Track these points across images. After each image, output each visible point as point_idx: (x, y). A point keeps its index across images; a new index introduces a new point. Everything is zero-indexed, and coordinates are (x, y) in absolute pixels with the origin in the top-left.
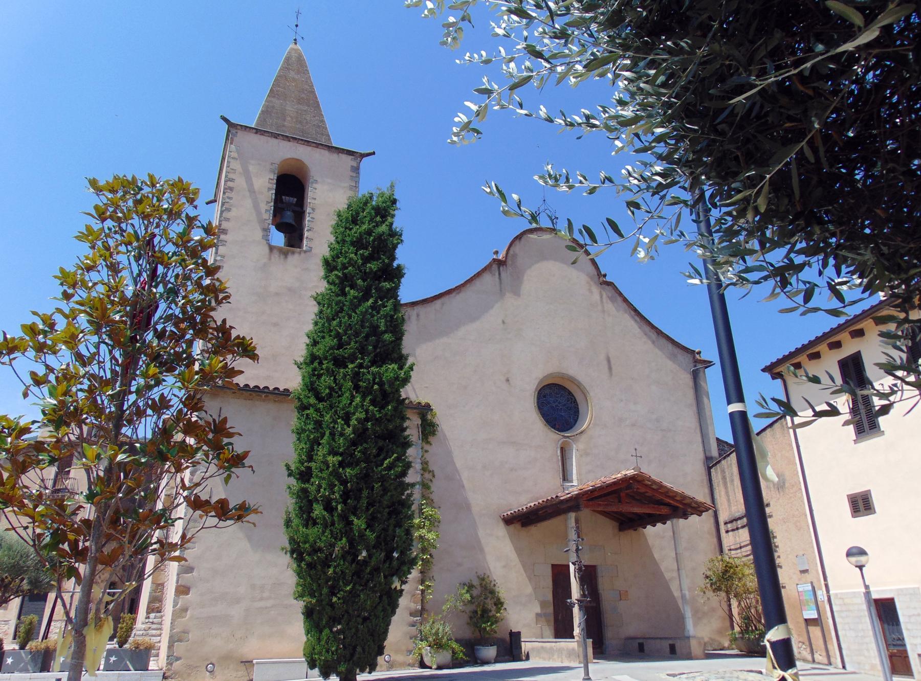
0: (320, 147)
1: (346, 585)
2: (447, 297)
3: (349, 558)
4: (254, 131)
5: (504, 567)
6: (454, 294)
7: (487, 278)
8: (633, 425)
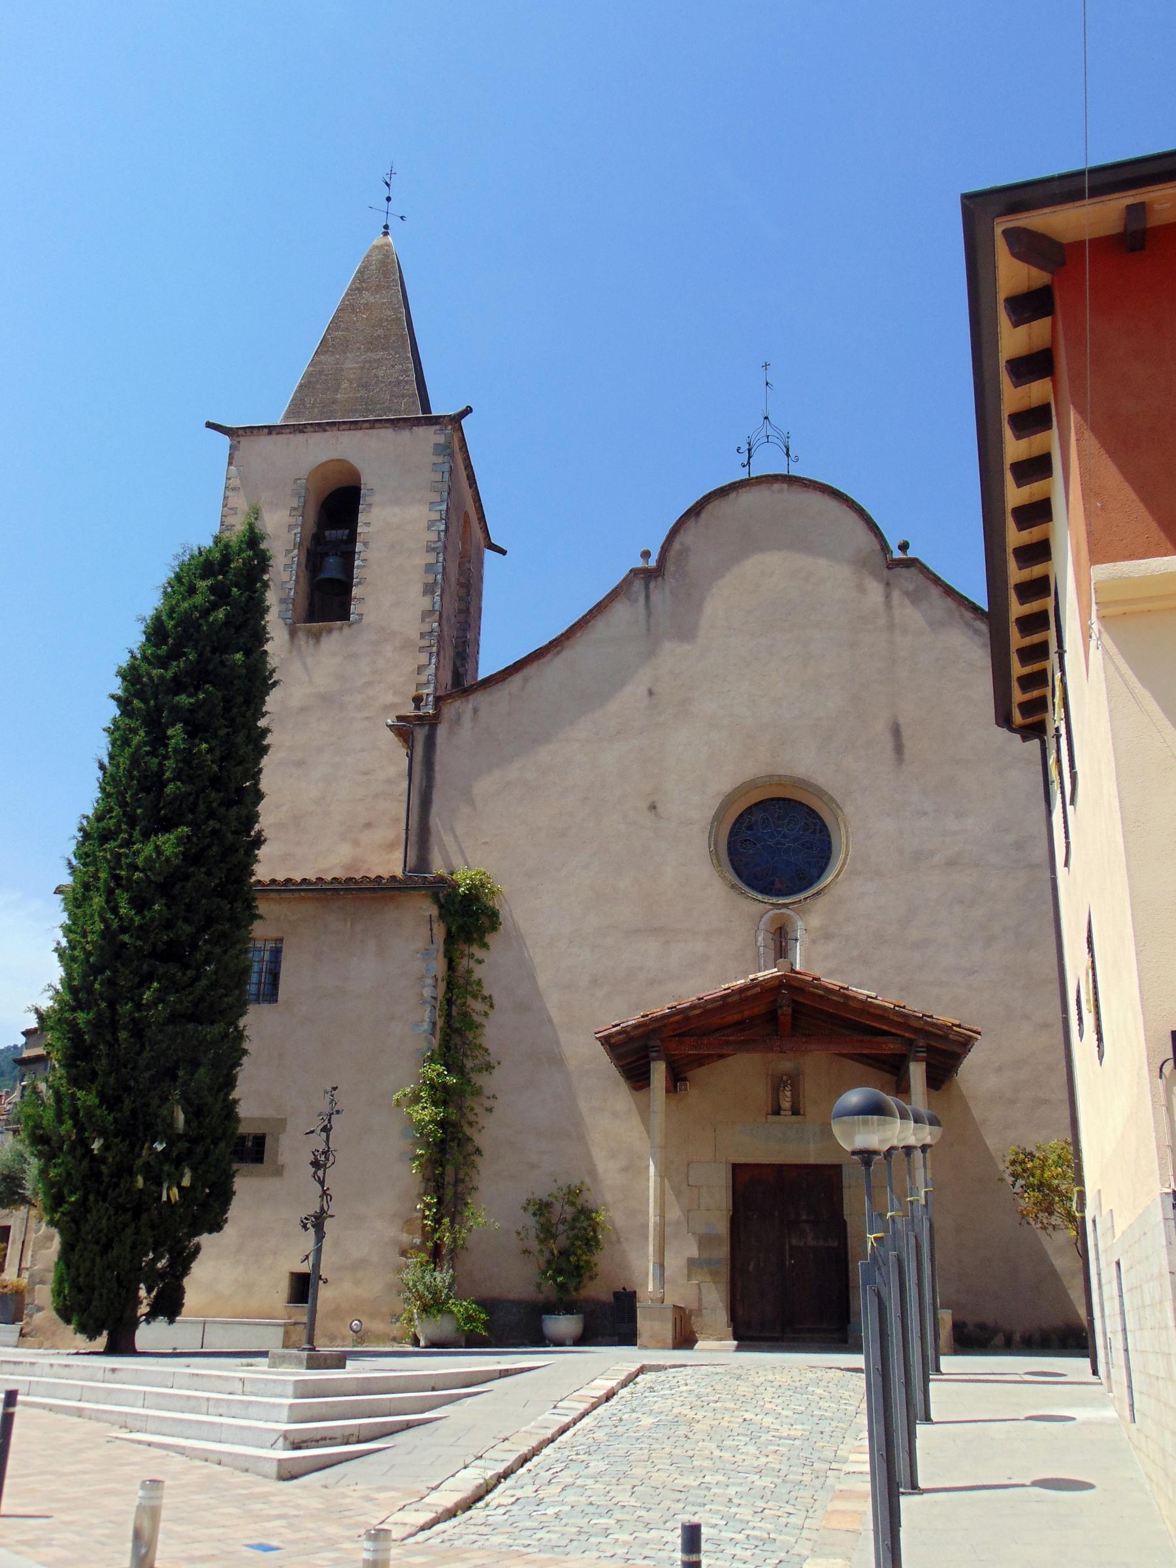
0: (377, 425)
1: (72, 1193)
2: (535, 665)
3: (79, 1152)
4: (266, 431)
5: (624, 1169)
6: (549, 657)
7: (621, 612)
8: (952, 863)
